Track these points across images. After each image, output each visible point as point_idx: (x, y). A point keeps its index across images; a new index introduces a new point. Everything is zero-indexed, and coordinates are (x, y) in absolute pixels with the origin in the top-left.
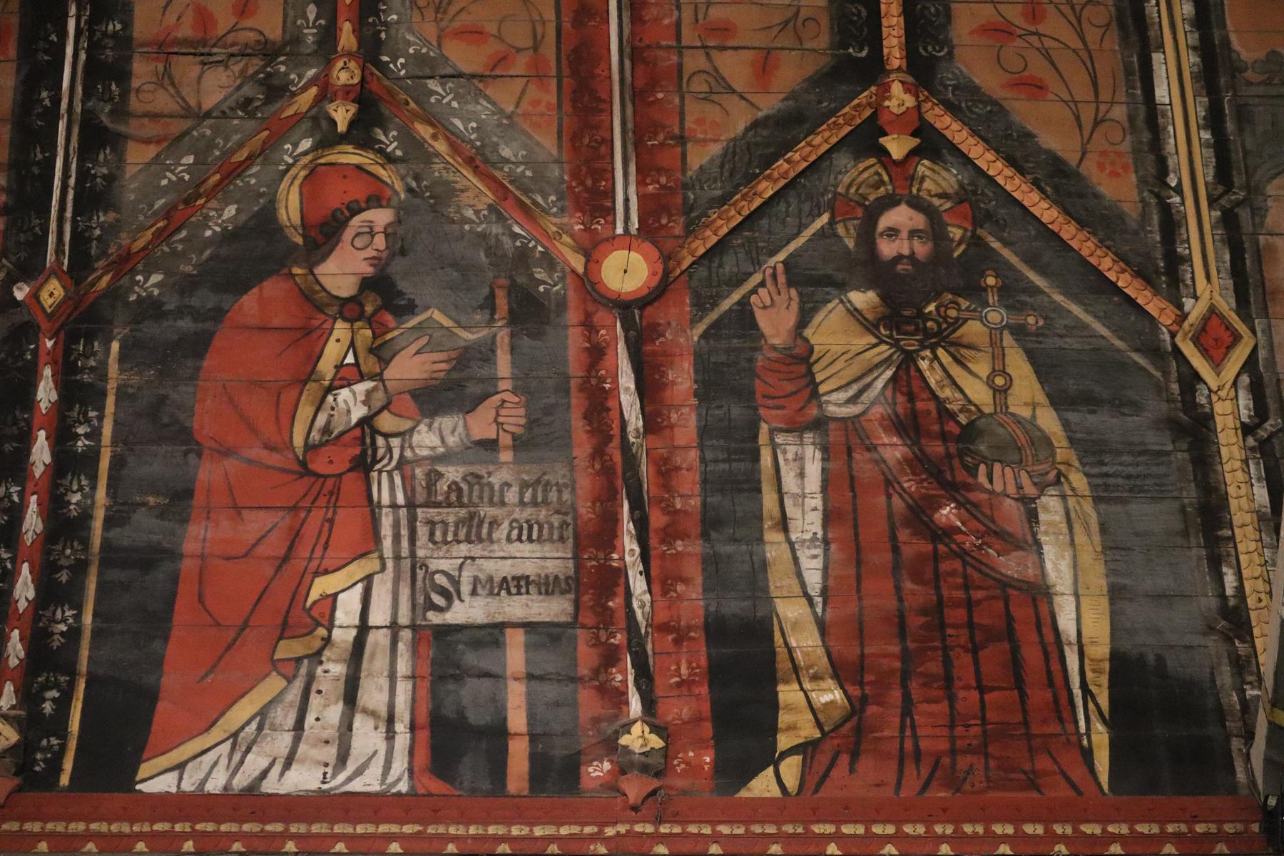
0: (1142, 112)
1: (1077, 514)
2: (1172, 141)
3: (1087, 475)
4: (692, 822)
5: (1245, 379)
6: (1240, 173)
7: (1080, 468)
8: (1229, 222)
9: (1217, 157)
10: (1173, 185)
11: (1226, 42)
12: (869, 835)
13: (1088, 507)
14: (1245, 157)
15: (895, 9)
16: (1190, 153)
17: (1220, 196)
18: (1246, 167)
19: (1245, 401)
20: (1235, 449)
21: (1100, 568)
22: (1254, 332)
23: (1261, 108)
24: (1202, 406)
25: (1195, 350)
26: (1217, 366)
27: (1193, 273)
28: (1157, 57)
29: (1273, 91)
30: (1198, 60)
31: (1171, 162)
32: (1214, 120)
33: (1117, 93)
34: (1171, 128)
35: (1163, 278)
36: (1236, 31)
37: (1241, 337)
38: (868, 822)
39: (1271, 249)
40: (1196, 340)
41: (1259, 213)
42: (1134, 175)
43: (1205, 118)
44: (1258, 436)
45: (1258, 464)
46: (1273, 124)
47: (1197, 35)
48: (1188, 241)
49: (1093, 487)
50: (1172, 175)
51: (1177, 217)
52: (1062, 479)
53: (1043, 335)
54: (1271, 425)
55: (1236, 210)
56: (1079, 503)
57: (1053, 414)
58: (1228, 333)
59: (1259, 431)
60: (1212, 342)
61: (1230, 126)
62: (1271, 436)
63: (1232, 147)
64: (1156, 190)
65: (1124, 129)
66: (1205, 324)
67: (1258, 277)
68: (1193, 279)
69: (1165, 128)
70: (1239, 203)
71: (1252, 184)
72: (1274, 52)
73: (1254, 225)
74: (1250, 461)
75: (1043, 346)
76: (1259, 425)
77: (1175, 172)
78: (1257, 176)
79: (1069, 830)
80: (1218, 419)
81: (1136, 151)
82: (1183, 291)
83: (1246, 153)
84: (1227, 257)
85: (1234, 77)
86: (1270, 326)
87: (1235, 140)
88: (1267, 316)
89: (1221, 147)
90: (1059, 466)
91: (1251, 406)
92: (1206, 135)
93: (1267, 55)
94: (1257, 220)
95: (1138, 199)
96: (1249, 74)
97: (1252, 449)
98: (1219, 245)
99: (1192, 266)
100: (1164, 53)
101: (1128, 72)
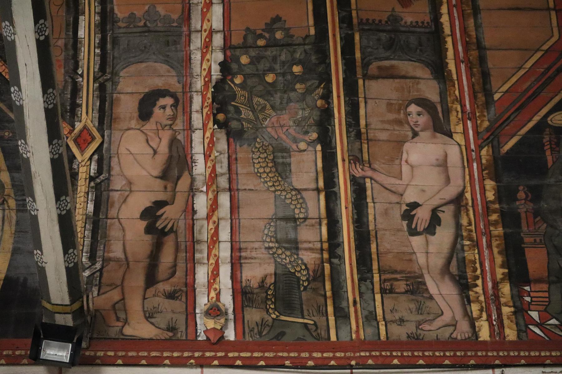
0: (71, 41)
1: (8, 217)
2: (83, 54)
3: (16, 200)
4: (373, 351)
5: (96, 157)
6: (110, 67)
7: (14, 197)
8: (102, 88)
9: (101, 60)
10: (80, 73)
11: (112, 10)
12: (413, 356)
13: (13, 214)
14: (113, 60)
16: (89, 59)
17: (99, 78)
18: (113, 64)
19: (94, 166)
20: (83, 187)
21: (11, 241)
22: (103, 136)
23: (124, 38)
24: (75, 169)
25: (74, 145)
26: (82, 151)
27: (81, 111)
28: (81, 18)
29: (130, 31)
30: (99, 18)
31: (80, 64)
32: (102, 45)
33: (61, 34)
34: (83, 49)
35: (68, 114)
36: (118, 5)
37: (96, 138)
39: (118, 99)
40: (76, 141)
41: (115, 84)
42: (63, 69)
43: (98, 44)
44: (96, 182)
45: (93, 194)
46: (128, 45)
47: (100, 8)
48: (82, 97)
49: (17, 205)
50: (80, 69)
51: (79, 87)
52: (5, 202)
53: (11, 140)
54: (103, 177)
55: (105, 83)
56: (10, 212)
57: (8, 173)
58: (90, 137)
59: (97, 179)
60: (82, 141)
61: (109, 46)
62: (103, 181)
63: (108, 56)
64: (72, 76)
65: (62, 50)
66: (80, 134)
67: (110, 112)
68: (81, 114)
69: (80, 49)
70: (107, 80)
71: (114, 72)
72: (132, 13)
73: (112, 90)
74: (90, 193)
75: (9, 145)
76: (97, 177)
77: (82, 68)
78: (117, 68)
79: (399, 354)
80: (80, 174)
81: (66, 60)
82: (76, 119)
83: (114, 58)
84: (98, 104)
85: (113, 25)
86: (111, 134)
87: (110, 53)
88: (111, 129)
89: (103, 57)
90: (5, 197)
91: (96, 169)
92: (98, 51)
93: (129, 15)
94: (114, 87)
95: (63, 80)
96: (120, 24)
97: (92, 187)
98: (95, 98)
99: (82, 109)
100: (85, 16)
101: (68, 25)
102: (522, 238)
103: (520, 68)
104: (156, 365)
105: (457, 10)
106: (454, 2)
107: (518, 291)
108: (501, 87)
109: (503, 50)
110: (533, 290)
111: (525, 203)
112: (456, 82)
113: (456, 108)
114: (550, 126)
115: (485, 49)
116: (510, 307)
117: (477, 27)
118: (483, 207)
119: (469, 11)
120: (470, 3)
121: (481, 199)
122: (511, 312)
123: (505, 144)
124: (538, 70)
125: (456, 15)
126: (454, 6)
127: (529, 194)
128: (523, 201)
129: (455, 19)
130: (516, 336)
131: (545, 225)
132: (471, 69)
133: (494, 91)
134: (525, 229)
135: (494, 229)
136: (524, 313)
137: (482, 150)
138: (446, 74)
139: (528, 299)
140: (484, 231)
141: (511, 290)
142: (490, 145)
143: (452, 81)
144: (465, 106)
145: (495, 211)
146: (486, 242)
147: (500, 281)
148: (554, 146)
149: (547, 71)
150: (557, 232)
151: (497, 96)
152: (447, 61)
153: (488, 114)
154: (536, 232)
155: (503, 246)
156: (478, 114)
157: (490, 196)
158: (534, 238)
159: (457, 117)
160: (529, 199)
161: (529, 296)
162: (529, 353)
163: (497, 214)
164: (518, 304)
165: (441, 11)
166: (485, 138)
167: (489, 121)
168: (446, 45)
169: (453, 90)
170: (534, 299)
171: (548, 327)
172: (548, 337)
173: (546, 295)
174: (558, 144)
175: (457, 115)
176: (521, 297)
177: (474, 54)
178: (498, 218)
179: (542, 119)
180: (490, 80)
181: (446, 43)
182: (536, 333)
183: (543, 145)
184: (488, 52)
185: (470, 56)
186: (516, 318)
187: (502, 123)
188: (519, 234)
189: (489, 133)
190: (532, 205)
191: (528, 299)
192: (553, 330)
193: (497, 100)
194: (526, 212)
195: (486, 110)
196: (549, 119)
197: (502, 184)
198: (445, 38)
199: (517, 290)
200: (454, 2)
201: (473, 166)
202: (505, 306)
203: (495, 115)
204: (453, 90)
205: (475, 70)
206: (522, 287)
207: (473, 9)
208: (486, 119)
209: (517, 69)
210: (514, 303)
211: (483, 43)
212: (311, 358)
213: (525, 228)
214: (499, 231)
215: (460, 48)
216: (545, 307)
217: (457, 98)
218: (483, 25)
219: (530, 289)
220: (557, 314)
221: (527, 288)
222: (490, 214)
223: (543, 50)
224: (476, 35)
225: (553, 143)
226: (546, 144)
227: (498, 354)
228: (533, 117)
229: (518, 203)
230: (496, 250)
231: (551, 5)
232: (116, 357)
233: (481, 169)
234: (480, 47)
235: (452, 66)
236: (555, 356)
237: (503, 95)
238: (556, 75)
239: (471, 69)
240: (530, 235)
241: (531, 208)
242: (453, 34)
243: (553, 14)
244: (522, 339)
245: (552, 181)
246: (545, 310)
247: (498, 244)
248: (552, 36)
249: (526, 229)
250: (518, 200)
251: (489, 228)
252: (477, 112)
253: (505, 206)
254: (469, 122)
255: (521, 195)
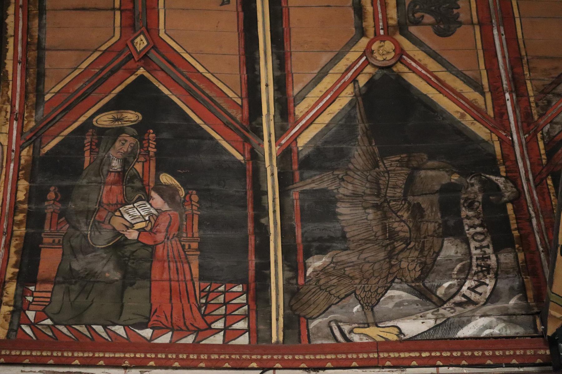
12: (146, 357)
15: (379, 1)
28: (377, 58)
38: (145, 353)
102: (42, 238)
103: (76, 69)
104: (67, 365)
105: (22, 10)
106: (21, 3)
107: (23, 291)
108: (53, 88)
109: (62, 50)
110: (37, 290)
111: (53, 203)
112: (11, 83)
113: (6, 108)
114: (94, 127)
115: (44, 49)
116: (10, 306)
117: (41, 27)
118: (10, 207)
119: (35, 12)
120: (37, 4)
121: (10, 200)
122: (9, 311)
123: (46, 145)
124: (93, 70)
125: (21, 16)
126: (21, 6)
127: (59, 195)
128: (52, 202)
129: (19, 20)
130: (5, 335)
131: (68, 226)
132: (27, 69)
133: (46, 91)
134: (48, 229)
135: (17, 229)
136: (22, 312)
137: (22, 150)
138: (2, 74)
139: (30, 299)
140: (5, 230)
141: (16, 289)
142: (32, 145)
143: (7, 81)
144: (15, 106)
145: (22, 211)
146: (5, 241)
147: (8, 280)
148: (94, 147)
149: (100, 72)
150: (78, 233)
151: (47, 97)
152: (6, 61)
153: (36, 114)
154: (58, 232)
155: (22, 246)
156: (26, 115)
157: (21, 196)
158: (53, 239)
159: (5, 117)
160: (58, 200)
161: (32, 295)
162: (135, 355)
163: (23, 215)
164: (19, 304)
165: (7, 12)
166: (28, 138)
167: (36, 121)
168: (7, 46)
169: (7, 90)
170: (36, 299)
171: (40, 327)
172: (36, 337)
173: (49, 295)
174: (98, 145)
175: (6, 115)
176: (23, 296)
177: (33, 55)
178: (23, 219)
179: (87, 120)
180: (44, 81)
181: (8, 44)
182: (26, 332)
183: (84, 146)
184: (46, 53)
185: (29, 57)
186: (12, 317)
187: (47, 124)
188: (40, 234)
189: (32, 134)
190: (60, 205)
191: (30, 299)
192: (44, 330)
193: (47, 101)
194: (52, 213)
195: (34, 111)
196: (95, 120)
197: (34, 185)
198: (7, 39)
199: (22, 289)
200: (21, 3)
201: (10, 166)
202: (6, 305)
203: (43, 116)
204: (7, 90)
205: (32, 70)
206: (27, 287)
207: (39, 10)
208: (33, 119)
209: (74, 70)
210: (15, 302)
211: (44, 44)
212: (177, 359)
213: (47, 229)
214: (21, 231)
215: (20, 49)
216: (44, 307)
217: (9, 99)
218: (47, 26)
219: (35, 289)
220: (54, 314)
221: (32, 288)
222: (17, 214)
223: (101, 51)
224: (39, 36)
225: (94, 144)
226: (86, 145)
227: (73, 354)
228: (79, 118)
229: (46, 204)
230: (13, 250)
231: (117, 5)
232: (199, 360)
233: (18, 169)
234: (40, 48)
235: (9, 67)
236: (35, 356)
237: (54, 96)
238: (109, 76)
239: (27, 69)
240: (50, 235)
241: (58, 208)
242: (15, 36)
243: (118, 14)
244: (10, 338)
245: (84, 182)
246: (43, 311)
247: (17, 244)
248: (114, 36)
249: (48, 229)
250: (48, 201)
251: (13, 228)
252: (25, 112)
253: (33, 207)
254: (15, 122)
255: (51, 195)
